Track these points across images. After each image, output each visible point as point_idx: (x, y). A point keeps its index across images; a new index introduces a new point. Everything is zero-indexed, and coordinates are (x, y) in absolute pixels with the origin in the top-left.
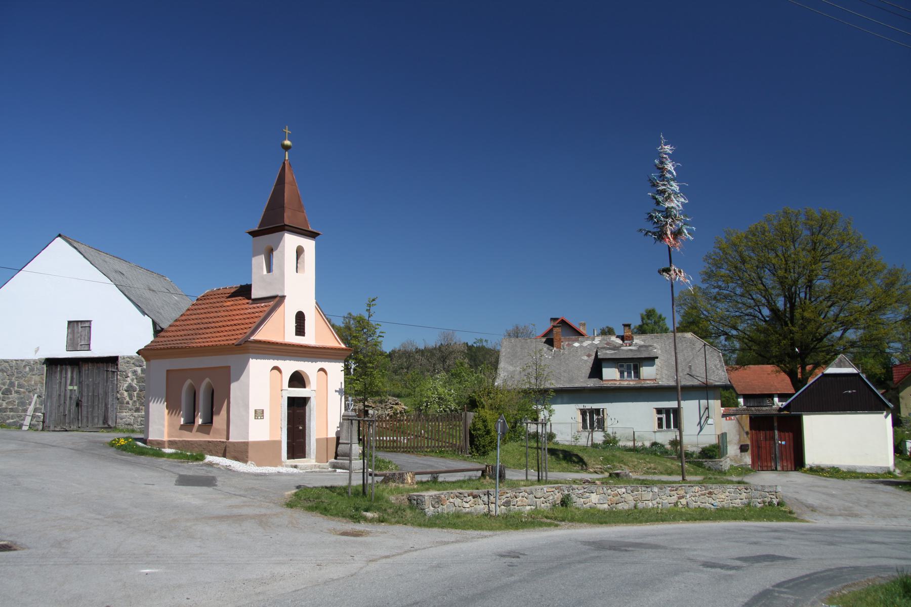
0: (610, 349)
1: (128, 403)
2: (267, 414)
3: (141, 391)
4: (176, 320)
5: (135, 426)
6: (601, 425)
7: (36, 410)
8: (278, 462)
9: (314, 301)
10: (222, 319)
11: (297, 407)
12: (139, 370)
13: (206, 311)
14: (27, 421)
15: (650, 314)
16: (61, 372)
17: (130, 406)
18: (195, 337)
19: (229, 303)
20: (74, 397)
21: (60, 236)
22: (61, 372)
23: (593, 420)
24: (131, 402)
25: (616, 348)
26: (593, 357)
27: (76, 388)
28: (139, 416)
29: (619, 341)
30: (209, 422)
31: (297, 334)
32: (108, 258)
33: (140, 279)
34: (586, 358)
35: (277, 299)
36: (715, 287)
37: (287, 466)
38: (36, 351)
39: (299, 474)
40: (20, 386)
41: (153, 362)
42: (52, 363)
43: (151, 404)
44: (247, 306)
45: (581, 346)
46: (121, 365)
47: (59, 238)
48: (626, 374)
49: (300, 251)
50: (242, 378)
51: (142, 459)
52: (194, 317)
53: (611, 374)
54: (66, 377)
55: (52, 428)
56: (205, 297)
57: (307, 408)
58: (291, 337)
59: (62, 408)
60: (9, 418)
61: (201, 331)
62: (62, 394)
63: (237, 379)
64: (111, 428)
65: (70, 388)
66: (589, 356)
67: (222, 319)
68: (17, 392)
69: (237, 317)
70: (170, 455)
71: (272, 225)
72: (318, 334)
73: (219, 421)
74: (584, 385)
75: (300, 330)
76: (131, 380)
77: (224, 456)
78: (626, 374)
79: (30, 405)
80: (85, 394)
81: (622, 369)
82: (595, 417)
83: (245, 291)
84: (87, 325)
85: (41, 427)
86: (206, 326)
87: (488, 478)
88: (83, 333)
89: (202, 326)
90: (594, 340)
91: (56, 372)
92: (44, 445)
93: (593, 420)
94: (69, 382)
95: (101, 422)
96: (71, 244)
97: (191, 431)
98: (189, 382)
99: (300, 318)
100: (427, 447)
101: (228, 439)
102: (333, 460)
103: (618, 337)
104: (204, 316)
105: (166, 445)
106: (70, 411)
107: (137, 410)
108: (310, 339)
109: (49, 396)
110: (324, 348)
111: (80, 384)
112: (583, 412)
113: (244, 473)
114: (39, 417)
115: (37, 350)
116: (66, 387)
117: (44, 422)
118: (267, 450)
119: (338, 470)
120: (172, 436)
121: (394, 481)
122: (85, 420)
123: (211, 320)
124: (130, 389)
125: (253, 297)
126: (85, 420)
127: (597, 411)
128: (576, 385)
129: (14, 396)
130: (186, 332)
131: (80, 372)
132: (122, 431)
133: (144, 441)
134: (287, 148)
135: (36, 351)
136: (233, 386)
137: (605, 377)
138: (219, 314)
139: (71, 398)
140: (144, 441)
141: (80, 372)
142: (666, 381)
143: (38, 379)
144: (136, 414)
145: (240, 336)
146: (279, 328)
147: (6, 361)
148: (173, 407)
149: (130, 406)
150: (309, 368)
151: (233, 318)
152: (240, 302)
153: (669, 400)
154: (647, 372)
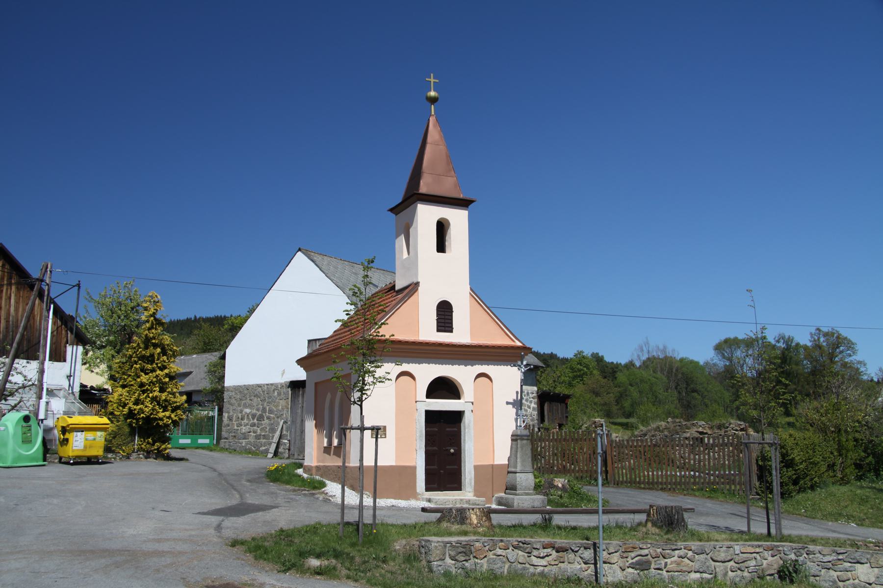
2: (391, 432)
9: (469, 287)
21: (300, 250)
31: (438, 330)
38: (283, 374)
40: (271, 412)
47: (299, 253)
49: (442, 228)
68: (268, 418)
85: (287, 455)
108: (462, 333)
110: (487, 347)
117: (289, 450)
118: (396, 479)
121: (449, 521)
129: (266, 421)
134: (433, 100)
135: (283, 374)
146: (416, 322)
147: (259, 386)
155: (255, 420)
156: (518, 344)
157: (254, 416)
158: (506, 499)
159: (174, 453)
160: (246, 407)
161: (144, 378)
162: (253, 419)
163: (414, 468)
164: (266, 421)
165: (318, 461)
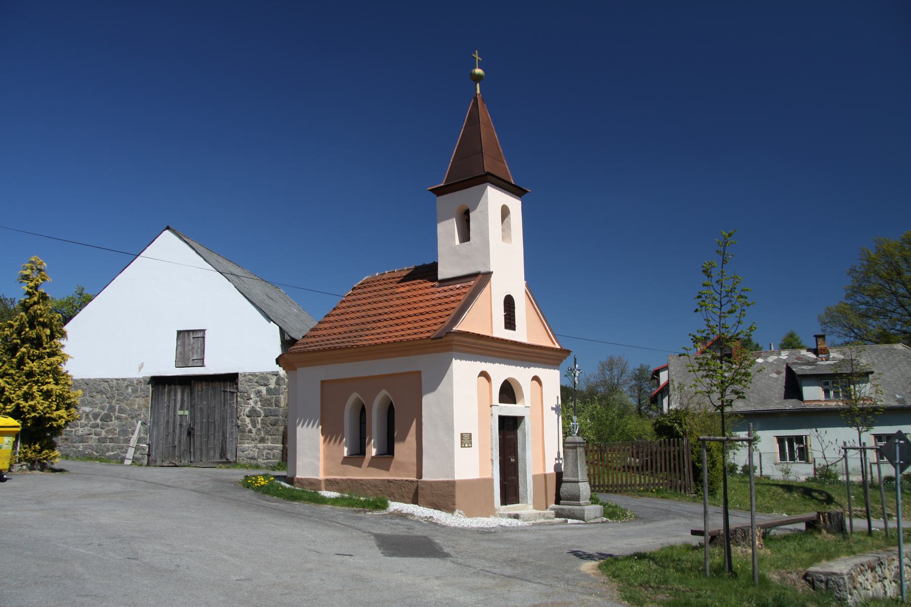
0: (804, 364)
1: (250, 431)
3: (266, 416)
4: (313, 330)
5: (260, 461)
6: (804, 455)
7: (140, 440)
8: (489, 511)
10: (397, 309)
11: (509, 427)
12: (264, 389)
13: (370, 300)
14: (130, 454)
15: (792, 335)
16: (169, 393)
17: (253, 435)
18: (361, 333)
19: (402, 289)
20: (184, 424)
21: (168, 228)
22: (169, 393)
23: (795, 449)
24: (254, 430)
25: (809, 363)
26: (784, 374)
27: (187, 413)
28: (264, 448)
29: (812, 356)
30: (388, 450)
31: (506, 327)
32: (220, 259)
33: (258, 289)
34: (775, 375)
35: (480, 277)
36: (862, 304)
37: (502, 516)
38: (140, 369)
39: (523, 530)
40: (122, 411)
41: (300, 370)
42: (159, 382)
43: (299, 429)
44: (433, 290)
45: (766, 362)
46: (242, 385)
47: (167, 231)
48: (832, 393)
50: (441, 387)
51: (297, 506)
52: (353, 309)
53: (813, 394)
54: (175, 400)
55: (159, 463)
56: (364, 285)
57: (519, 432)
58: (500, 331)
59: (170, 438)
60: (108, 450)
61: (369, 326)
62: (171, 421)
63: (433, 388)
64: (230, 462)
65: (180, 413)
66: (778, 373)
67: (397, 309)
68: (118, 418)
69: (421, 305)
70: (335, 501)
71: (468, 177)
72: (529, 329)
73: (404, 450)
74: (781, 407)
75: (510, 323)
76: (253, 403)
77: (415, 501)
78: (832, 393)
79: (133, 434)
80: (198, 420)
81: (827, 387)
82: (796, 446)
83: (428, 272)
84: (200, 335)
85: (145, 462)
86: (375, 318)
87: (824, 531)
88: (196, 346)
89: (369, 319)
90: (780, 354)
91: (163, 394)
92: (157, 485)
93: (795, 449)
94: (178, 405)
95: (218, 455)
96: (180, 238)
97: (360, 467)
98: (354, 396)
99: (509, 303)
100: (639, 485)
101: (419, 475)
102: (553, 505)
103: (809, 350)
104: (369, 307)
105: (323, 485)
106: (180, 441)
107: (262, 440)
109: (155, 423)
111: (192, 408)
112: (780, 440)
113: (455, 528)
114: (143, 449)
115: (141, 367)
116: (175, 411)
117: (149, 455)
119: (570, 521)
120: (332, 474)
122: (198, 453)
123: (380, 311)
124: (253, 414)
125: (440, 277)
126: (198, 453)
127: (799, 439)
128: (771, 408)
129: (115, 422)
130: (345, 329)
131: (192, 393)
132: (244, 466)
133: (291, 480)
134: (478, 78)
135: (140, 369)
136: (428, 401)
137: (806, 396)
138: (391, 303)
139: (181, 425)
140: (291, 480)
141: (192, 393)
142: (885, 401)
143: (142, 402)
144: (260, 445)
145: (435, 327)
146: (483, 318)
147: (105, 381)
148: (330, 432)
149: (253, 435)
150: (522, 375)
151: (415, 305)
152: (420, 286)
153: (891, 425)
154: (865, 390)
155: (98, 421)
156: (558, 346)
157: (96, 416)
158: (569, 510)
159: (58, 463)
160: (85, 405)
161: (30, 365)
162: (95, 419)
163: (493, 480)
164: (115, 422)
165: (325, 474)
